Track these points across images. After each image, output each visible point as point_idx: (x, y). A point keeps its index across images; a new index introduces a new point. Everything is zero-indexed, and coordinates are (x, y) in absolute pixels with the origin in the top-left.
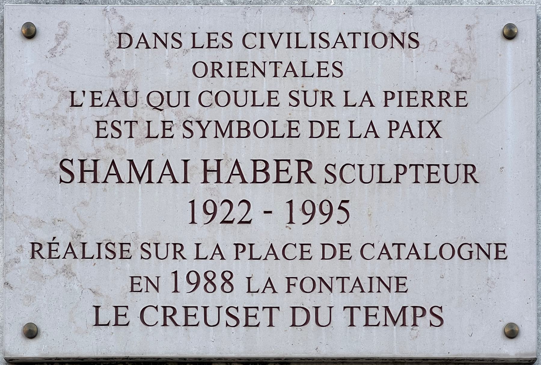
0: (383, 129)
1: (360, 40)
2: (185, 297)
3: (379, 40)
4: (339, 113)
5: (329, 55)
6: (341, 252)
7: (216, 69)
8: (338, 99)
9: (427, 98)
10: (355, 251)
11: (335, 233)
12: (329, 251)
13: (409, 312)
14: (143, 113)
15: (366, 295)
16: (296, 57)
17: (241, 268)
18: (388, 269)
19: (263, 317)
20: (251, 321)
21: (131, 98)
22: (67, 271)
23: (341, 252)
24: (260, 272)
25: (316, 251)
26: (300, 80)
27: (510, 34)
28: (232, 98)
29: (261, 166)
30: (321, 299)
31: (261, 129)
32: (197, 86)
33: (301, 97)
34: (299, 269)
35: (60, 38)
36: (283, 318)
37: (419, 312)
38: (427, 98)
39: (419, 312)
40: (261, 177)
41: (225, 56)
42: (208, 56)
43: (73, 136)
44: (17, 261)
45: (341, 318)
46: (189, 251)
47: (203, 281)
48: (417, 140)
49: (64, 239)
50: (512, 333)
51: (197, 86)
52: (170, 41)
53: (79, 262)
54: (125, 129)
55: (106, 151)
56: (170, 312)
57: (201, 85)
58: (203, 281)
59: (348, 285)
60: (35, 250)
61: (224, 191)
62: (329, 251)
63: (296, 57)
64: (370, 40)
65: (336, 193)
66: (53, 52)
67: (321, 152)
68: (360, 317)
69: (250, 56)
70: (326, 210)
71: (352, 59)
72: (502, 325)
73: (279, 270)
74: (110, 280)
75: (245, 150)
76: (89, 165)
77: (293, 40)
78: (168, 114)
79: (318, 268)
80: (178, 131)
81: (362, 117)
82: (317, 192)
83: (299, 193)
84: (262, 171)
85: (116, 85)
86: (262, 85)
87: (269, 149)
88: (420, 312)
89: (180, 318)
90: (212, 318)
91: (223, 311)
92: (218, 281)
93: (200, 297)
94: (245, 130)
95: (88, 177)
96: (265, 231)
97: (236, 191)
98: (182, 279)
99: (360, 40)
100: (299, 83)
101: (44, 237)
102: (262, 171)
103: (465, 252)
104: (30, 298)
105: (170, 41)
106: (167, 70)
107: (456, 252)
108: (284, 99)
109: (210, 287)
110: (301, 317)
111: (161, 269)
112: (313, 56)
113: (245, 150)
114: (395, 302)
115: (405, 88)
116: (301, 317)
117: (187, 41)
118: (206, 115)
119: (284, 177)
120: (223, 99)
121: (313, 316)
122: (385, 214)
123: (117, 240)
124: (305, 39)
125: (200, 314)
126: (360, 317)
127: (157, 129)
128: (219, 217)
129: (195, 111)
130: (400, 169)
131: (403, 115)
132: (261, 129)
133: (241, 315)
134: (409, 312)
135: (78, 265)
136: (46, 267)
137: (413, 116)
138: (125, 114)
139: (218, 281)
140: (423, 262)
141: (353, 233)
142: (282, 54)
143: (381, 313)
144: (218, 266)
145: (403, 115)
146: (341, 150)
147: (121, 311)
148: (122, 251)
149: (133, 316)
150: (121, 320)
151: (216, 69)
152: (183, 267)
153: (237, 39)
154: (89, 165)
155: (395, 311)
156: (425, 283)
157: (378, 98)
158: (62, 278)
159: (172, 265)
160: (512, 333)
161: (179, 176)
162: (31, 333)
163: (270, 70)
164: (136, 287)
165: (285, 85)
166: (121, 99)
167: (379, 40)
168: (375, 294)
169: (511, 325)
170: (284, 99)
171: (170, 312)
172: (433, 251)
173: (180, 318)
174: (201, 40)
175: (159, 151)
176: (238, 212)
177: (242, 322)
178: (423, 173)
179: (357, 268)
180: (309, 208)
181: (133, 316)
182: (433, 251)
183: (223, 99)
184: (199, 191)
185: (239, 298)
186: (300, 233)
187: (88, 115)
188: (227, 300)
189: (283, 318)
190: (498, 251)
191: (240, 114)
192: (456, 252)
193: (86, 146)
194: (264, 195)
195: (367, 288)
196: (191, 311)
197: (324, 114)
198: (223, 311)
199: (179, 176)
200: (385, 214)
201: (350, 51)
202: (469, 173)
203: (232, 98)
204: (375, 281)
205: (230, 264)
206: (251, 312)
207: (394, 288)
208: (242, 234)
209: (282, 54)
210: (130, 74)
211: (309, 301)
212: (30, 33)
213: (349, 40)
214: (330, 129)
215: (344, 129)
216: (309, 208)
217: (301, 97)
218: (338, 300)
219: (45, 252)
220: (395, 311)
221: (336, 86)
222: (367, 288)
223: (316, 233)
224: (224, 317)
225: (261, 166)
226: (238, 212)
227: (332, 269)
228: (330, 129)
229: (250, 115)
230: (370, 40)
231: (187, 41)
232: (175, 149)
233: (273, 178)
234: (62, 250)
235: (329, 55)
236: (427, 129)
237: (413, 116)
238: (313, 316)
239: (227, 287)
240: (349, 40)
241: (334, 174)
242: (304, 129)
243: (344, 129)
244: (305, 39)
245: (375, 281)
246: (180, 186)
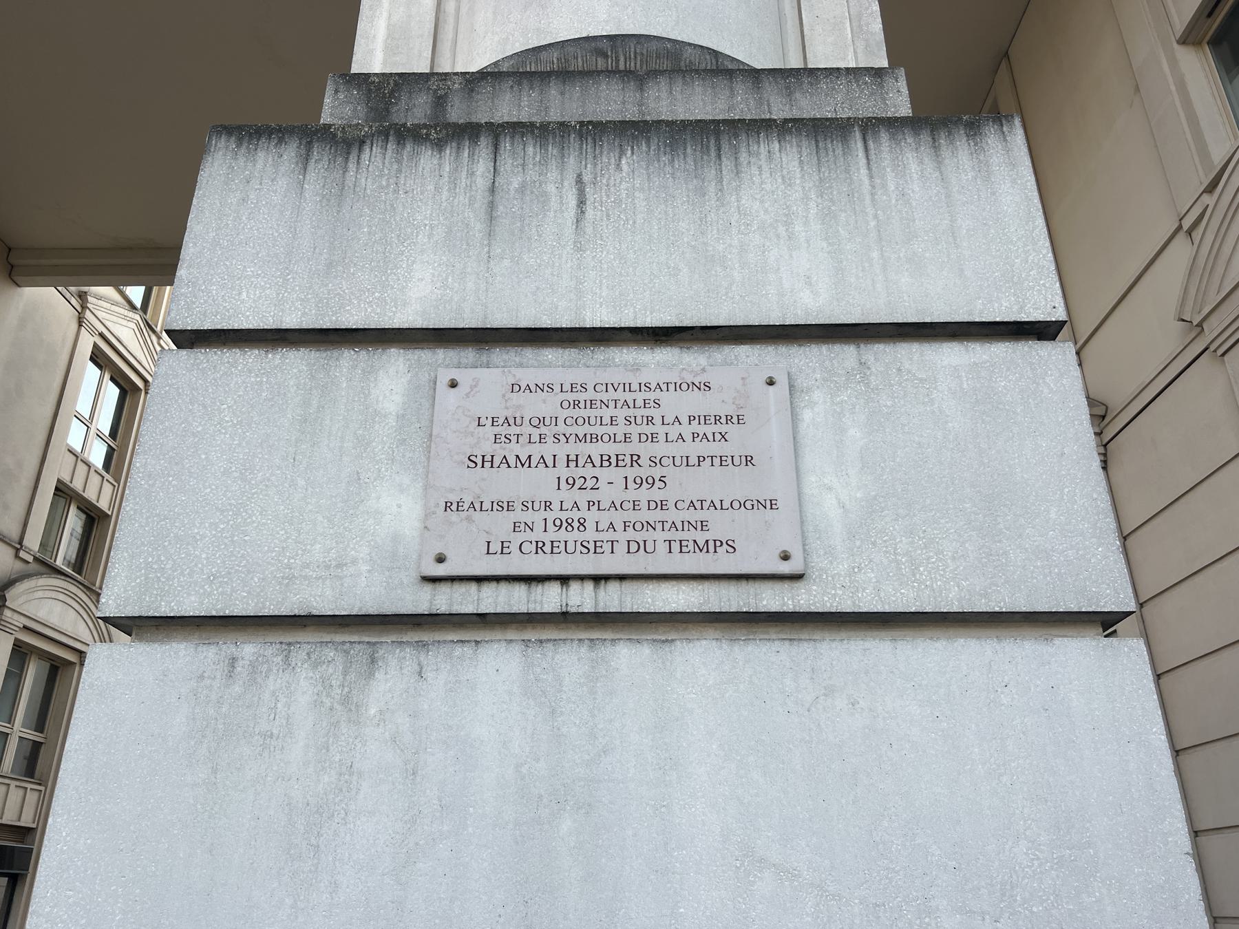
0: (688, 438)
1: (672, 387)
2: (552, 534)
3: (684, 386)
4: (658, 428)
5: (651, 396)
6: (662, 505)
7: (576, 404)
8: (658, 420)
9: (717, 419)
10: (671, 505)
11: (657, 495)
12: (653, 505)
13: (711, 544)
14: (527, 429)
15: (680, 532)
16: (629, 397)
17: (592, 516)
18: (694, 516)
19: (607, 547)
20: (598, 550)
21: (519, 421)
22: (469, 519)
23: (662, 505)
24: (605, 518)
25: (644, 505)
26: (632, 410)
27: (771, 383)
28: (587, 421)
29: (605, 458)
30: (649, 535)
31: (606, 438)
32: (563, 414)
33: (530, 505)
34: (632, 516)
35: (472, 388)
36: (621, 548)
37: (718, 543)
38: (717, 419)
39: (718, 543)
40: (606, 464)
41: (582, 397)
42: (571, 397)
43: (478, 443)
44: (434, 513)
45: (662, 548)
46: (556, 506)
47: (565, 524)
48: (711, 443)
49: (468, 500)
50: (785, 557)
51: (563, 414)
52: (546, 388)
53: (478, 513)
54: (514, 439)
55: (499, 451)
56: (540, 545)
57: (566, 413)
58: (565, 524)
59: (667, 526)
60: (448, 506)
61: (580, 472)
62: (653, 505)
63: (629, 397)
64: (678, 387)
65: (657, 472)
66: (467, 395)
67: (646, 450)
68: (676, 547)
69: (599, 396)
70: (650, 481)
71: (666, 398)
72: (778, 552)
73: (618, 518)
74: (500, 526)
75: (595, 450)
76: (488, 458)
77: (627, 387)
78: (543, 430)
79: (645, 515)
80: (550, 439)
81: (674, 431)
82: (644, 472)
83: (631, 473)
84: (605, 460)
85: (509, 413)
86: (607, 414)
87: (611, 449)
88: (718, 543)
89: (547, 548)
90: (570, 548)
91: (578, 544)
92: (576, 524)
93: (563, 535)
94: (595, 438)
95: (487, 465)
96: (606, 495)
97: (589, 471)
98: (550, 523)
99: (672, 387)
100: (631, 412)
101: (454, 498)
102: (605, 460)
103: (748, 505)
104: (442, 537)
105: (546, 388)
106: (545, 405)
107: (743, 505)
108: (621, 421)
109: (570, 528)
110: (634, 547)
111: (537, 518)
112: (639, 398)
113: (595, 450)
114: (701, 538)
115: (702, 414)
116: (634, 547)
117: (557, 388)
118: (568, 431)
119: (621, 463)
120: (580, 421)
121: (643, 546)
122: (685, 485)
123: (505, 500)
124: (635, 387)
125: (562, 545)
126: (676, 547)
127: (535, 438)
128: (577, 485)
129: (562, 427)
130: (701, 460)
131: (701, 429)
132: (606, 438)
133: (591, 546)
134: (711, 544)
135: (477, 515)
136: (454, 516)
137: (709, 430)
138: (514, 430)
139: (576, 524)
140: (719, 511)
141: (670, 495)
142: (621, 395)
143: (691, 544)
144: (576, 515)
145: (701, 429)
146: (660, 449)
147: (506, 545)
148: (509, 507)
149: (514, 548)
150: (505, 550)
151: (576, 404)
152: (551, 516)
153: (590, 387)
154: (488, 458)
155: (701, 543)
156: (720, 524)
157: (685, 420)
158: (465, 523)
159: (543, 514)
160: (785, 557)
161: (550, 463)
162: (441, 559)
163: (612, 404)
164: (684, 549)
165: (621, 413)
166: (511, 421)
167: (684, 386)
168: (686, 532)
169: (784, 552)
170: (621, 421)
171: (540, 545)
172: (726, 504)
173: (547, 548)
174: (567, 387)
175: (536, 451)
176: (590, 483)
177: (592, 550)
178: (717, 461)
179: (672, 515)
180: (638, 481)
181: (514, 548)
182: (726, 504)
183: (580, 421)
184: (563, 472)
185: (590, 535)
186: (632, 494)
187: (489, 431)
188: (581, 537)
189: (621, 548)
190: (773, 504)
191: (592, 430)
192: (743, 505)
193: (487, 448)
194: (605, 474)
195: (680, 528)
196: (555, 544)
197: (649, 429)
198: (578, 544)
199: (550, 463)
200: (685, 485)
201: (665, 393)
202: (749, 460)
203: (587, 421)
204: (686, 524)
205: (584, 513)
206: (598, 544)
207: (699, 528)
208: (594, 496)
209: (621, 395)
210: (519, 407)
211: (639, 537)
212: (453, 384)
213: (664, 387)
214: (653, 438)
215: (662, 438)
216: (638, 481)
217: (530, 505)
218: (660, 536)
219: (454, 507)
220: (701, 543)
221: (656, 413)
222: (680, 528)
223: (644, 494)
224: (579, 547)
225: (605, 458)
226: (590, 483)
227: (656, 515)
228: (653, 438)
229: (599, 430)
230: (678, 387)
231: (557, 388)
232: (548, 450)
233: (614, 463)
234: (466, 506)
235: (651, 396)
236: (718, 437)
237: (709, 430)
238: (643, 546)
239: (582, 528)
240: (664, 387)
241: (655, 462)
242: (635, 438)
243: (662, 438)
244: (635, 387)
245: (686, 524)
246: (551, 469)
